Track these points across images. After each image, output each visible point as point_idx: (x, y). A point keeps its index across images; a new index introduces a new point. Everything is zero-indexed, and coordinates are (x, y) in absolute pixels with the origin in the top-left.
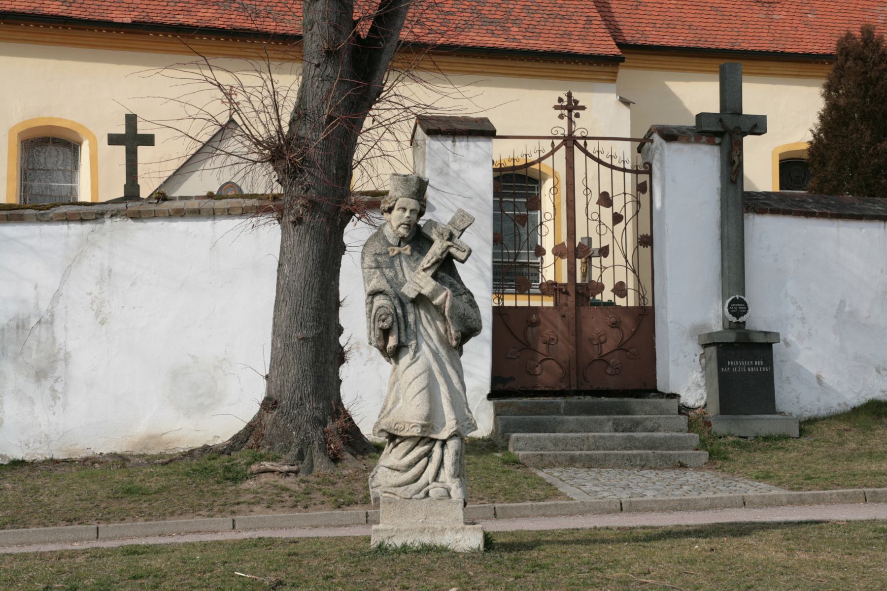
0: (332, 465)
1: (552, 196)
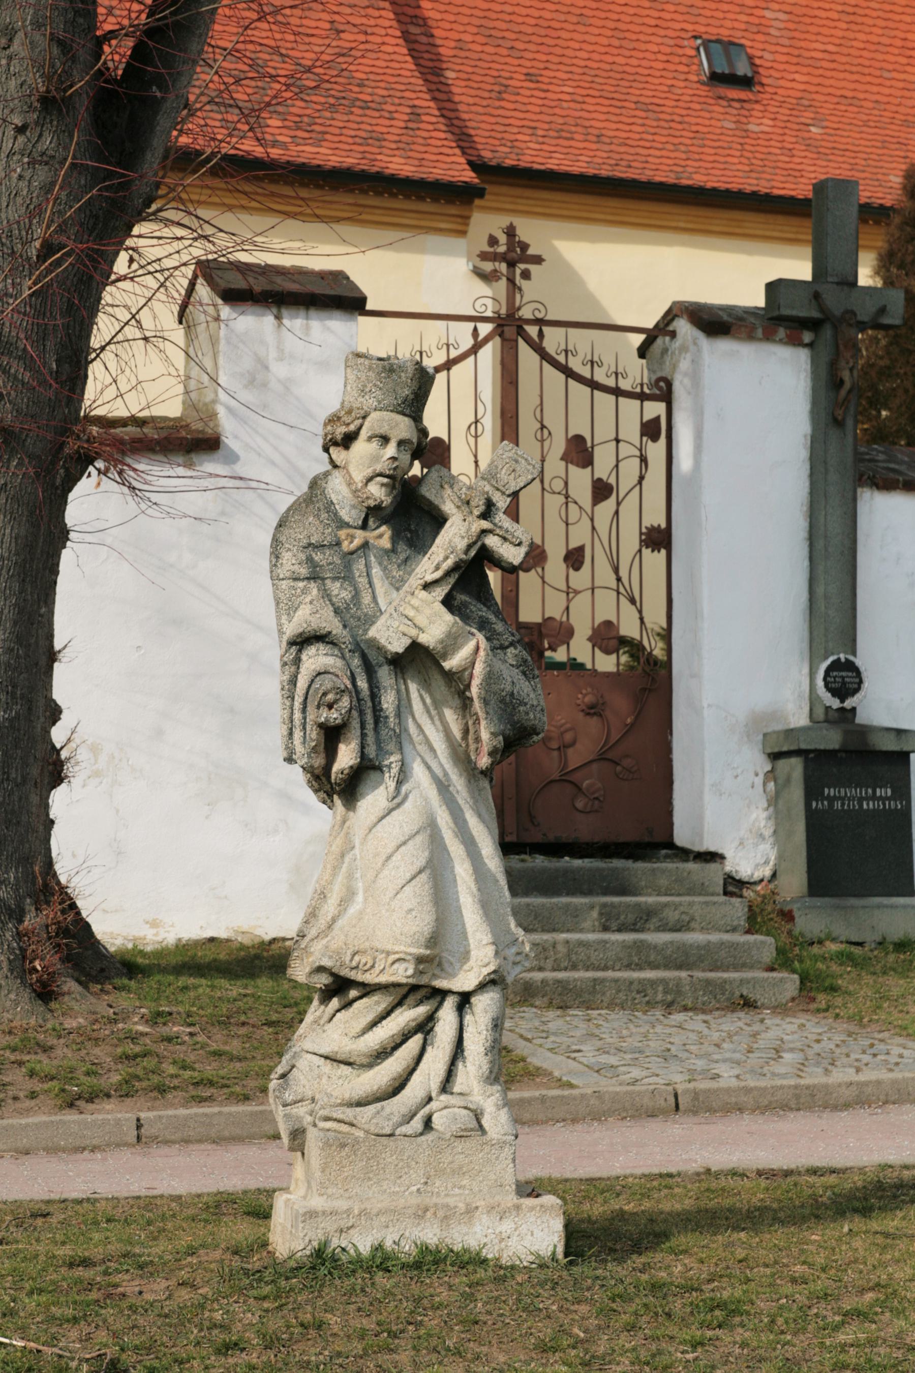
0: (40, 1007)
1: (472, 441)
